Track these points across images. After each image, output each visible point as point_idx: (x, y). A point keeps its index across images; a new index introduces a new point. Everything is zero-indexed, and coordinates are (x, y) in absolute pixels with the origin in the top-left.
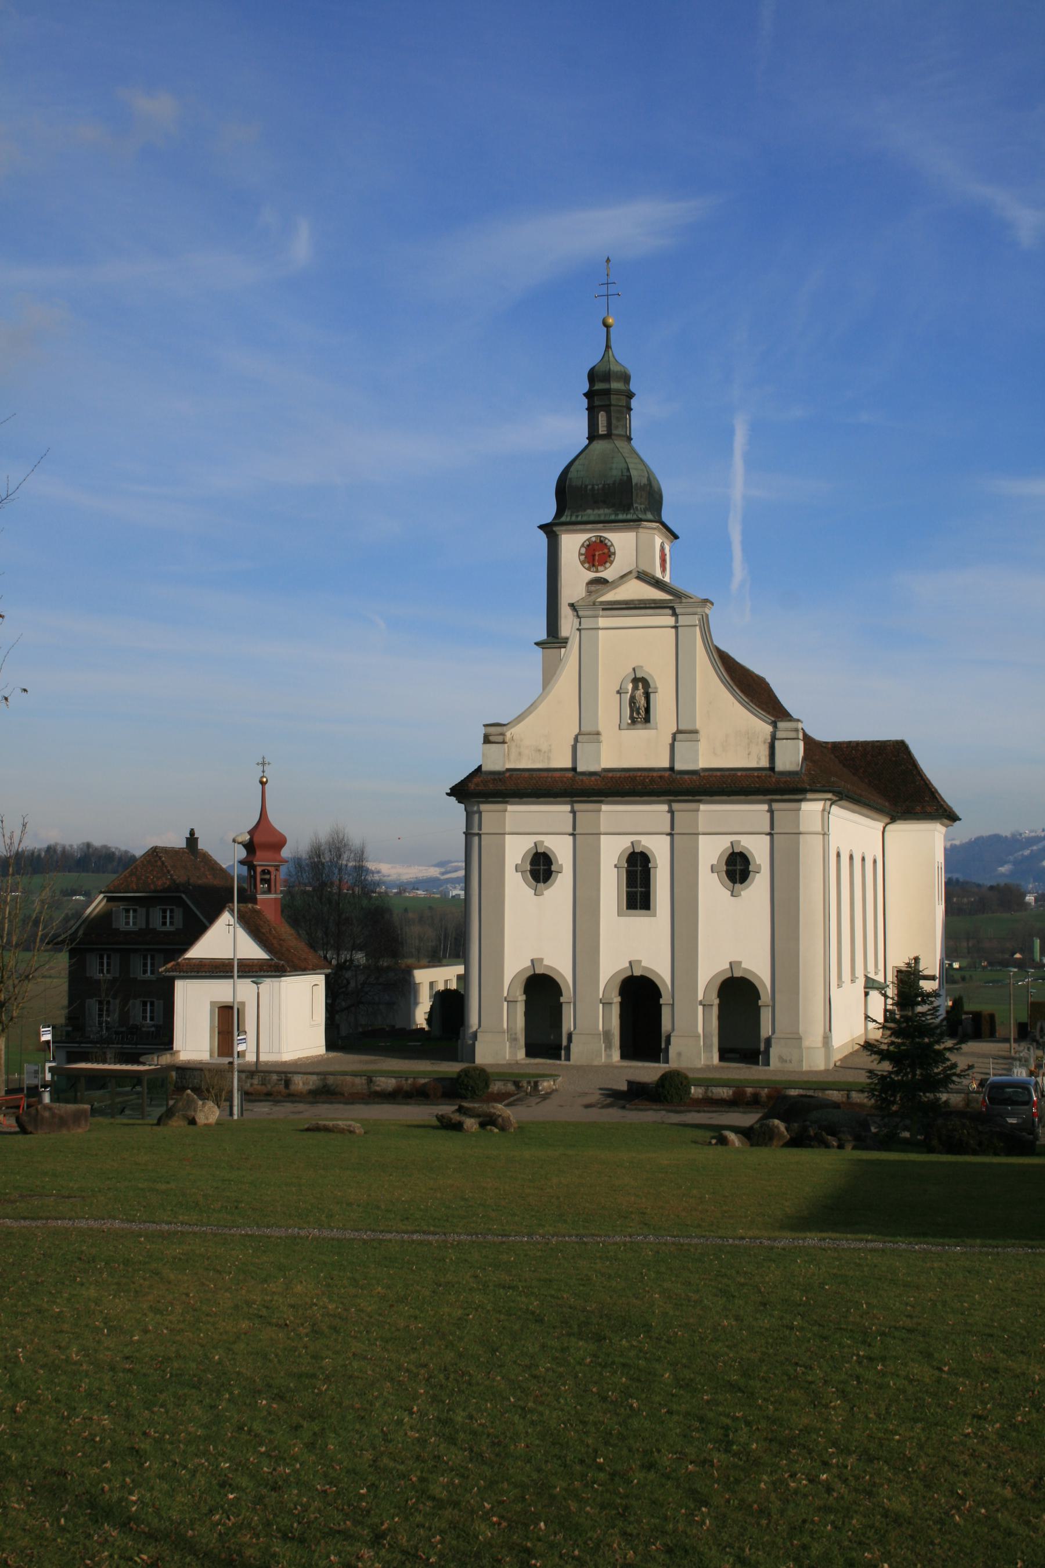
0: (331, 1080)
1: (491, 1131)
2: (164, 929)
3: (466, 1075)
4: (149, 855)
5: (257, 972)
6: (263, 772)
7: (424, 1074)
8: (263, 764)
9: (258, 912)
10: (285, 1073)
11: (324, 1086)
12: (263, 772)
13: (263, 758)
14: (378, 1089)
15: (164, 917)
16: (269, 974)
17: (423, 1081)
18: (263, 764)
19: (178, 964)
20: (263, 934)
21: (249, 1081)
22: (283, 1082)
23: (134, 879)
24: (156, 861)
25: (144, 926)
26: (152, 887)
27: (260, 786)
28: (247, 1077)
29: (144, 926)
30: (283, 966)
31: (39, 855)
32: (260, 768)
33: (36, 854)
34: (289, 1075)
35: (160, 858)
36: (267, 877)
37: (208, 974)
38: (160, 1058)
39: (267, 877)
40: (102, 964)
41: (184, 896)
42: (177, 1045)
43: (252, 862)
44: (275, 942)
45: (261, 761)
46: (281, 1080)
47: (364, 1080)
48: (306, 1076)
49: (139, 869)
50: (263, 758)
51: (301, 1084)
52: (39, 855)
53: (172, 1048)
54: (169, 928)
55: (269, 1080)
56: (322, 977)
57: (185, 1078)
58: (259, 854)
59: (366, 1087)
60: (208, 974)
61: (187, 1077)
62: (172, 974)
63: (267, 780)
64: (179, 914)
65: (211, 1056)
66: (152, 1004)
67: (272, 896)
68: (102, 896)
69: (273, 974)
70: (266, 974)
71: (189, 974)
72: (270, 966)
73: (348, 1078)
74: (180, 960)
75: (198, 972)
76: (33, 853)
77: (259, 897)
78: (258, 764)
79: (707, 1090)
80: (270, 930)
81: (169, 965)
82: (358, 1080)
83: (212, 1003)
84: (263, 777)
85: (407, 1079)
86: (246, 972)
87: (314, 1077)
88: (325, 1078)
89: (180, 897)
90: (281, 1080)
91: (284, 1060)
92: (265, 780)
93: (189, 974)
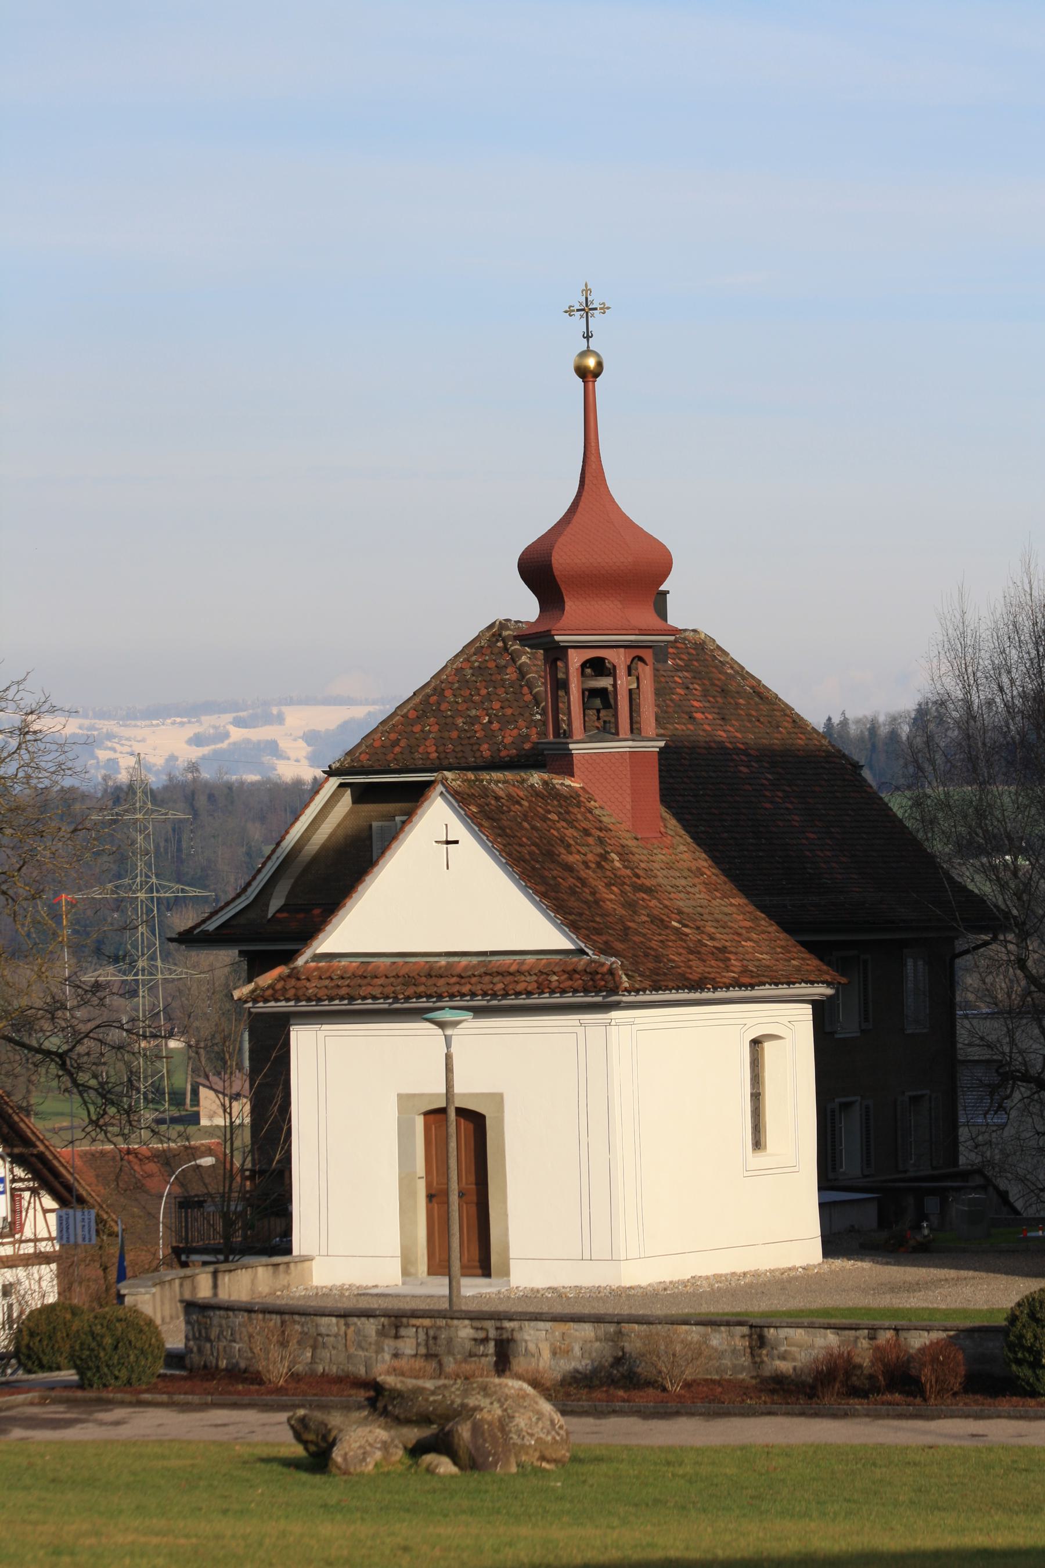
0: (635, 1339)
1: (430, 1471)
3: (1032, 1316)
4: (480, 651)
5: (529, 994)
6: (588, 336)
7: (922, 1320)
8: (587, 310)
9: (569, 801)
10: (497, 1317)
11: (618, 1361)
12: (588, 336)
13: (587, 291)
14: (784, 1367)
16: (569, 999)
17: (917, 1341)
18: (587, 310)
19: (295, 974)
20: (569, 868)
21: (389, 1344)
22: (491, 1347)
23: (431, 726)
26: (485, 750)
28: (382, 1333)
30: (611, 972)
31: (894, 735)
32: (578, 323)
33: (884, 731)
34: (507, 1324)
36: (605, 682)
37: (381, 1004)
38: (225, 1279)
39: (605, 682)
42: (302, 1239)
43: (548, 634)
44: (610, 898)
45: (577, 300)
46: (485, 1340)
47: (738, 1339)
48: (561, 1328)
49: (448, 693)
50: (587, 291)
51: (546, 1354)
52: (894, 735)
53: (288, 1251)
55: (450, 1340)
56: (806, 1012)
57: (208, 1339)
58: (573, 607)
59: (745, 1361)
60: (381, 1004)
61: (214, 1333)
62: (272, 1007)
63: (600, 365)
65: (405, 1273)
67: (623, 746)
68: (334, 782)
69: (580, 999)
70: (557, 999)
71: (326, 1006)
72: (572, 973)
73: (694, 1333)
74: (300, 961)
75: (351, 999)
76: (873, 729)
77: (577, 748)
78: (570, 312)
79: (35, 1246)
80: (604, 857)
81: (266, 979)
82: (718, 1339)
83: (404, 1100)
84: (587, 353)
85: (873, 1332)
86: (494, 996)
87: (587, 1330)
88: (619, 1333)
90: (485, 1340)
91: (627, 1283)
92: (591, 362)
93: (326, 1006)
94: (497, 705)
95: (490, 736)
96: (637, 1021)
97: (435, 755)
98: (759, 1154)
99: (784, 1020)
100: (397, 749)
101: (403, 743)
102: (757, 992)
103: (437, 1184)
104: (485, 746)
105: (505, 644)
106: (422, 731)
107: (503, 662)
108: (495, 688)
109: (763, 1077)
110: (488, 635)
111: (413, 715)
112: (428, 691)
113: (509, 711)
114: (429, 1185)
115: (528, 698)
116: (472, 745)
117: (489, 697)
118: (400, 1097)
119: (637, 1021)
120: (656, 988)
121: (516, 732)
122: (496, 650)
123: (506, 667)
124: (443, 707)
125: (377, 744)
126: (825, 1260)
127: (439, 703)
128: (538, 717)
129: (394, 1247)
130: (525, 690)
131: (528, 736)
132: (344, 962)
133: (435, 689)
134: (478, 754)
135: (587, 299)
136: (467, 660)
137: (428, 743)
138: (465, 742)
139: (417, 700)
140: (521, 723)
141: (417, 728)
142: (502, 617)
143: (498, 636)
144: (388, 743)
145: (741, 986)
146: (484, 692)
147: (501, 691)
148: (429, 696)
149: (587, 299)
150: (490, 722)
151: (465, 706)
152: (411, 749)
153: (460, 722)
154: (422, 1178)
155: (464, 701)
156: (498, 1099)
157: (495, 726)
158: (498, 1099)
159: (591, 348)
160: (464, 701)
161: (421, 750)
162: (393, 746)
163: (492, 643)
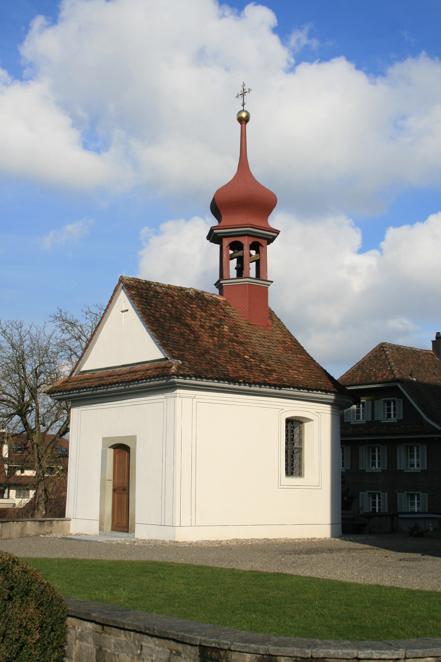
2: (388, 421)
4: (376, 351)
6: (243, 105)
15: (389, 410)
18: (243, 94)
24: (381, 355)
25: (370, 420)
26: (373, 379)
27: (239, 125)
29: (370, 420)
35: (385, 352)
40: (374, 457)
41: (399, 385)
54: (393, 419)
64: (400, 403)
65: (101, 529)
66: (418, 496)
89: (397, 388)
92: (244, 115)
94: (378, 366)
95: (375, 374)
96: (197, 397)
97: (359, 381)
98: (294, 481)
99: (314, 411)
100: (349, 380)
101: (351, 378)
102: (284, 391)
103: (117, 484)
104: (373, 378)
105: (383, 348)
106: (357, 374)
107: (382, 354)
108: (378, 361)
109: (304, 440)
110: (379, 346)
111: (355, 370)
112: (360, 363)
113: (381, 367)
114: (114, 485)
115: (387, 363)
116: (369, 377)
117: (376, 364)
118: (103, 438)
119: (197, 397)
120: (199, 376)
121: (382, 373)
122: (380, 351)
123: (382, 355)
124: (363, 367)
125: (344, 378)
126: (340, 543)
127: (363, 366)
128: (389, 368)
129: (96, 515)
130: (387, 361)
131: (385, 374)
132: (87, 374)
133: (362, 362)
134: (371, 380)
135: (243, 88)
136: (372, 354)
137: (357, 378)
138: (368, 377)
139: (357, 366)
140: (384, 371)
141: (355, 374)
142: (384, 342)
143: (382, 347)
144: (347, 378)
145: (275, 386)
146: (375, 362)
147: (380, 362)
148: (360, 364)
149: (243, 88)
150: (376, 371)
151: (370, 366)
152: (353, 379)
153: (367, 371)
154: (111, 480)
155: (370, 365)
156: (134, 438)
157: (377, 371)
158: (134, 438)
159: (245, 109)
160: (370, 365)
161: (355, 379)
162: (348, 379)
163: (380, 348)
